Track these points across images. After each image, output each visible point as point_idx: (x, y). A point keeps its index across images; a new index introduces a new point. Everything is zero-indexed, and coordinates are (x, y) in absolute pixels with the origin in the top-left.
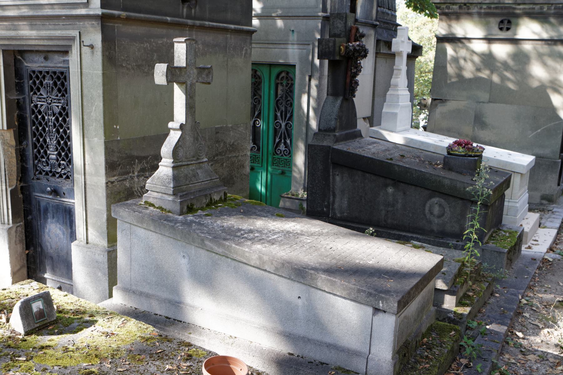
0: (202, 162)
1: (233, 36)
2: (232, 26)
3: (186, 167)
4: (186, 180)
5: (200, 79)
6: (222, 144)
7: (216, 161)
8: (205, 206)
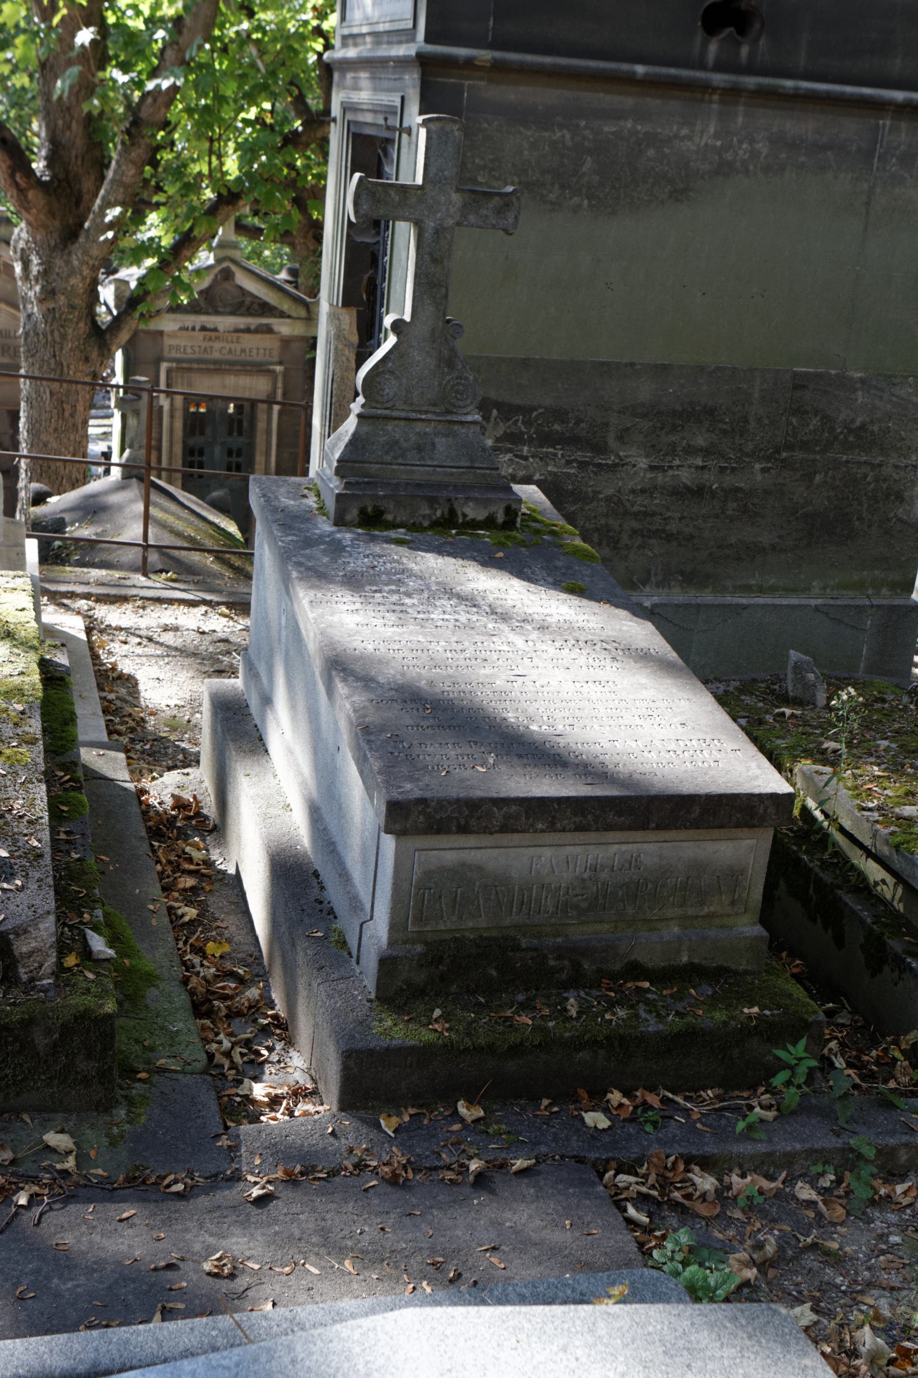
0: (462, 423)
1: (903, 125)
2: (899, 96)
3: (402, 423)
4: (387, 453)
5: (472, 218)
6: (815, 422)
7: (783, 461)
8: (426, 523)
